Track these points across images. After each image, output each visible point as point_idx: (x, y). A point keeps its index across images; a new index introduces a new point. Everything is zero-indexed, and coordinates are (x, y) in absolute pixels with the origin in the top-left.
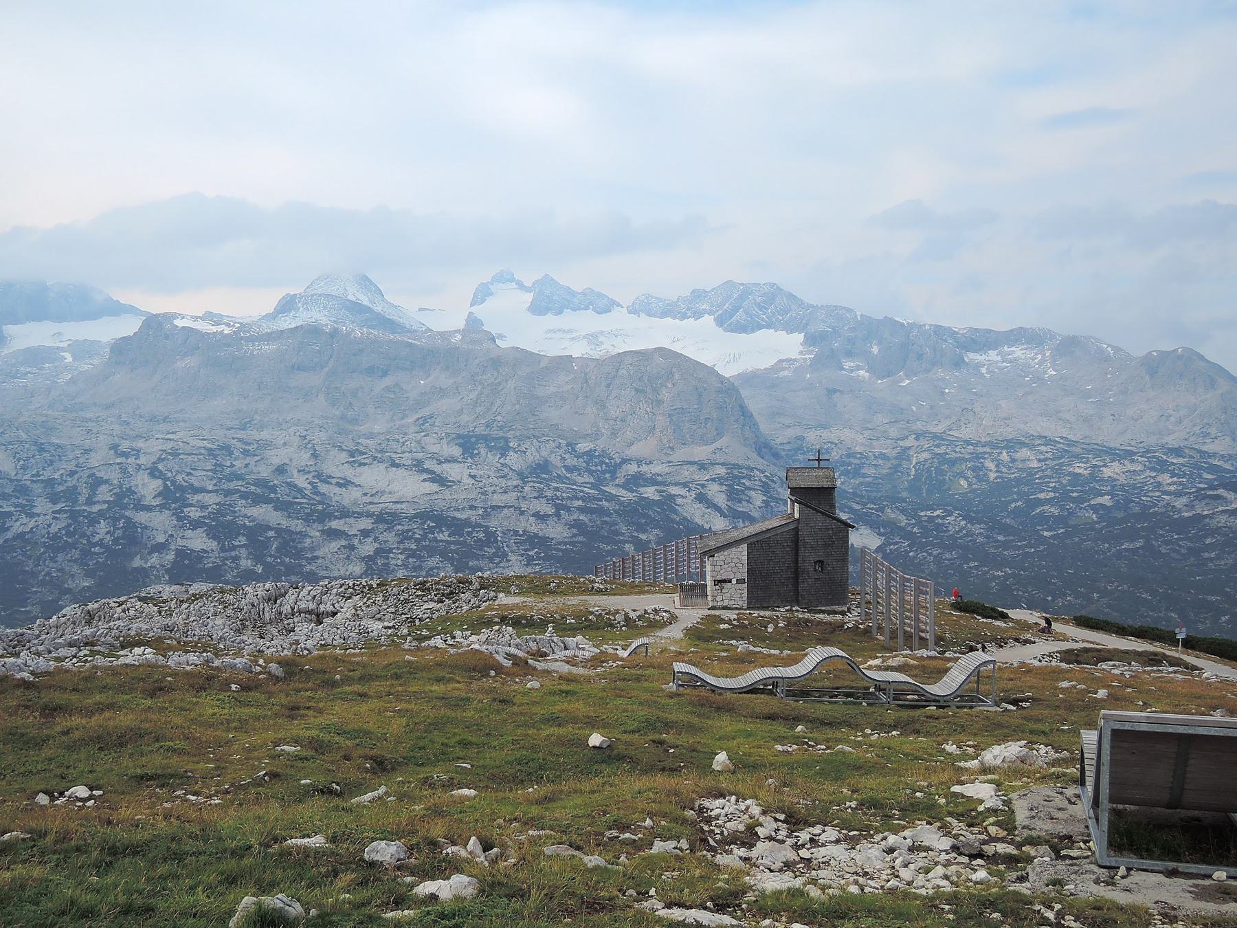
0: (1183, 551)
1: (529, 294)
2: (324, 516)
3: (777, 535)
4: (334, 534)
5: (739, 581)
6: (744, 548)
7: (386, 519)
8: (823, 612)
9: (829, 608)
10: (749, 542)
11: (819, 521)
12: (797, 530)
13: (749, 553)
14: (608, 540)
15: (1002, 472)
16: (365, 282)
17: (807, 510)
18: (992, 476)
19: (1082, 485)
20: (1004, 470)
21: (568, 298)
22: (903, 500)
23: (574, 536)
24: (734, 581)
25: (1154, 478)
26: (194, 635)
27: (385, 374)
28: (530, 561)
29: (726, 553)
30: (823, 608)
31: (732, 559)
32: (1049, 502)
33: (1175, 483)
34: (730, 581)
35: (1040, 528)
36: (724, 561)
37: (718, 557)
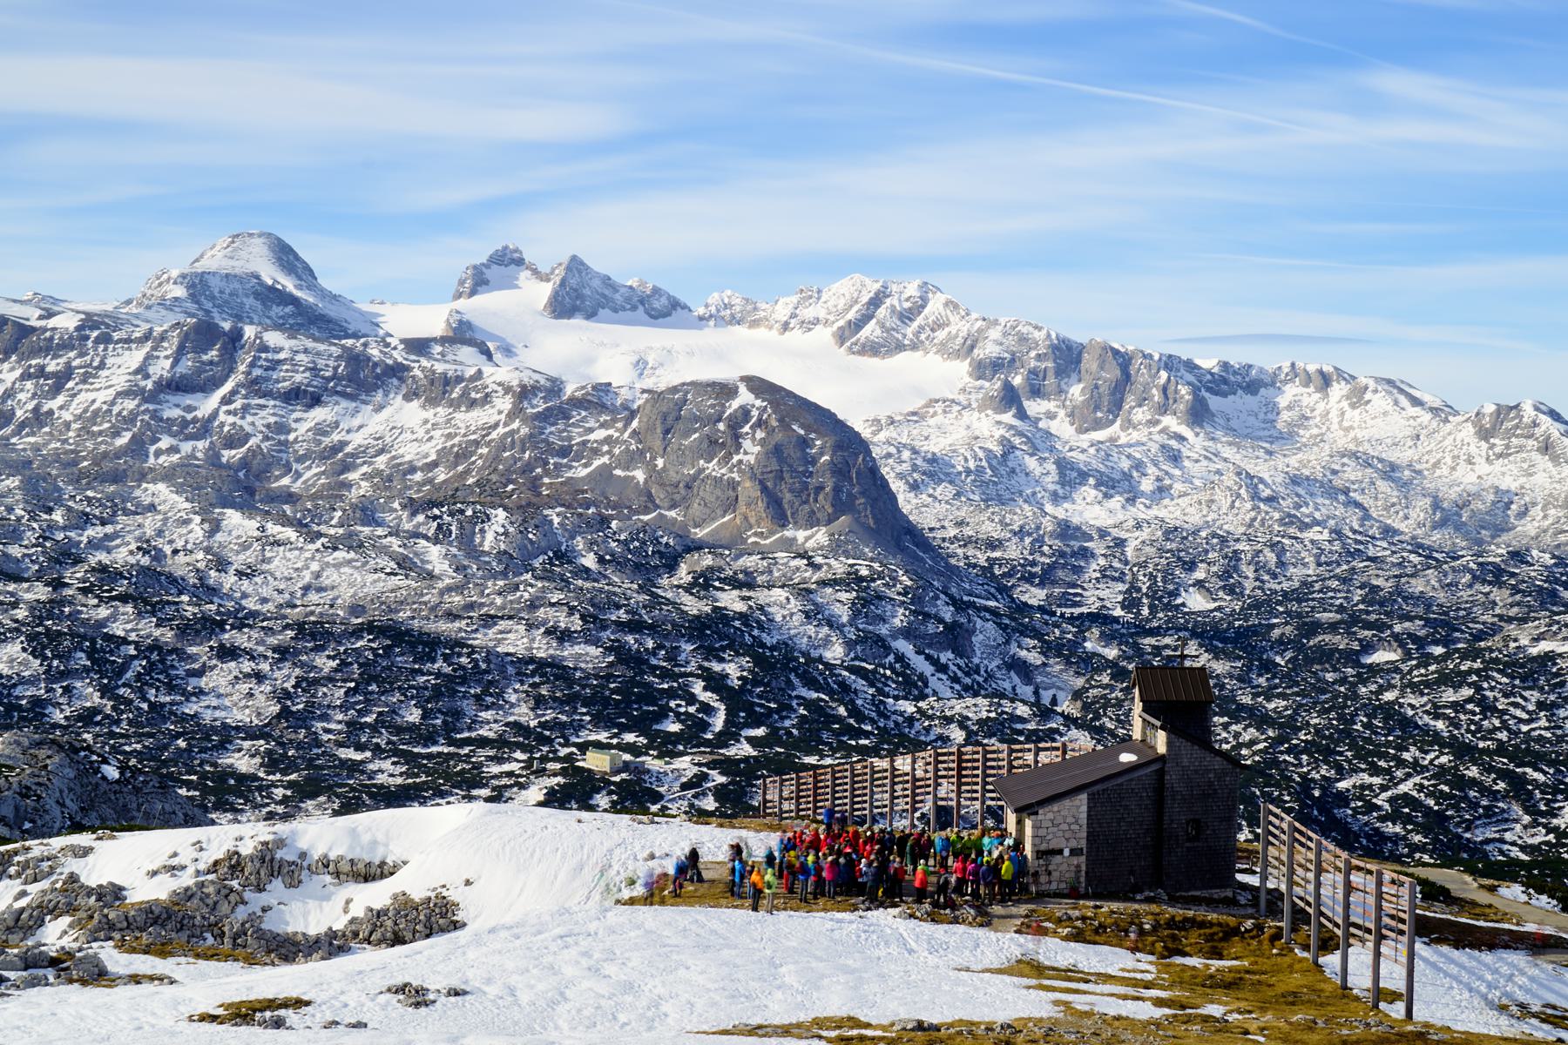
0: (1531, 707)
1: (544, 284)
2: (213, 626)
3: (1131, 780)
4: (228, 653)
5: (1074, 852)
6: (1082, 801)
7: (315, 633)
8: (1197, 901)
9: (1205, 893)
10: (1090, 790)
11: (1191, 754)
12: (1161, 774)
13: (1089, 812)
14: (665, 675)
15: (1263, 582)
16: (286, 256)
17: (1179, 742)
18: (1249, 585)
19: (1382, 604)
20: (1266, 577)
21: (607, 292)
22: (1116, 620)
23: (611, 664)
24: (1066, 852)
25: (1487, 594)
26: (194, 925)
27: (315, 401)
28: (539, 702)
29: (1056, 809)
30: (1197, 893)
31: (1065, 817)
32: (1333, 627)
33: (1518, 604)
34: (1060, 852)
35: (1318, 667)
36: (1052, 821)
37: (1045, 814)
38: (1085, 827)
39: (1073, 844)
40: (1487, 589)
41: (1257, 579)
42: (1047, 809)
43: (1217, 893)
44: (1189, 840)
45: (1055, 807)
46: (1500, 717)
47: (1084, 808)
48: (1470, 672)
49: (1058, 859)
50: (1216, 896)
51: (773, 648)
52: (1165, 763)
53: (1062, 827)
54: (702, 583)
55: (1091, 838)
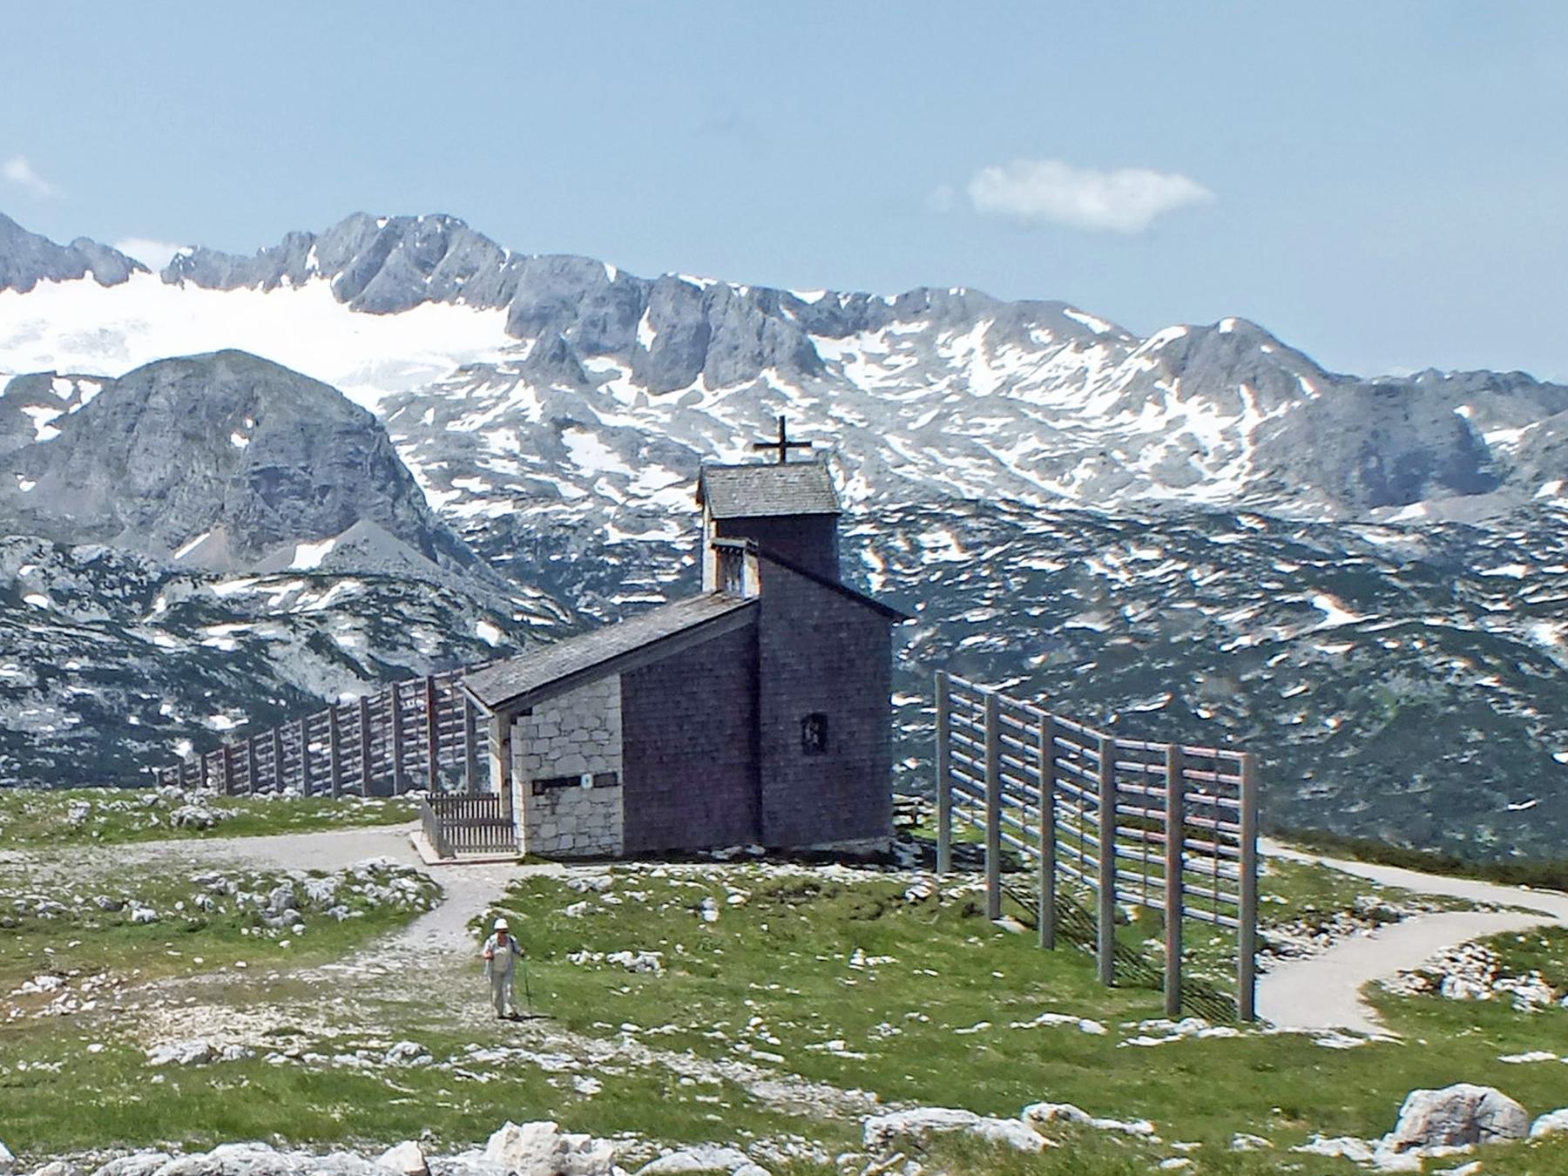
5: (601, 781)
12: (752, 636)
14: (138, 733)
34: (576, 781)
36: (558, 725)
38: (618, 735)
39: (600, 766)
40: (1182, 566)
41: (885, 571)
42: (546, 705)
43: (860, 846)
44: (806, 752)
45: (563, 701)
46: (1204, 728)
47: (616, 700)
48: (1166, 672)
49: (570, 794)
50: (860, 851)
51: (277, 696)
52: (759, 611)
53: (575, 736)
54: (186, 618)
55: (632, 752)
